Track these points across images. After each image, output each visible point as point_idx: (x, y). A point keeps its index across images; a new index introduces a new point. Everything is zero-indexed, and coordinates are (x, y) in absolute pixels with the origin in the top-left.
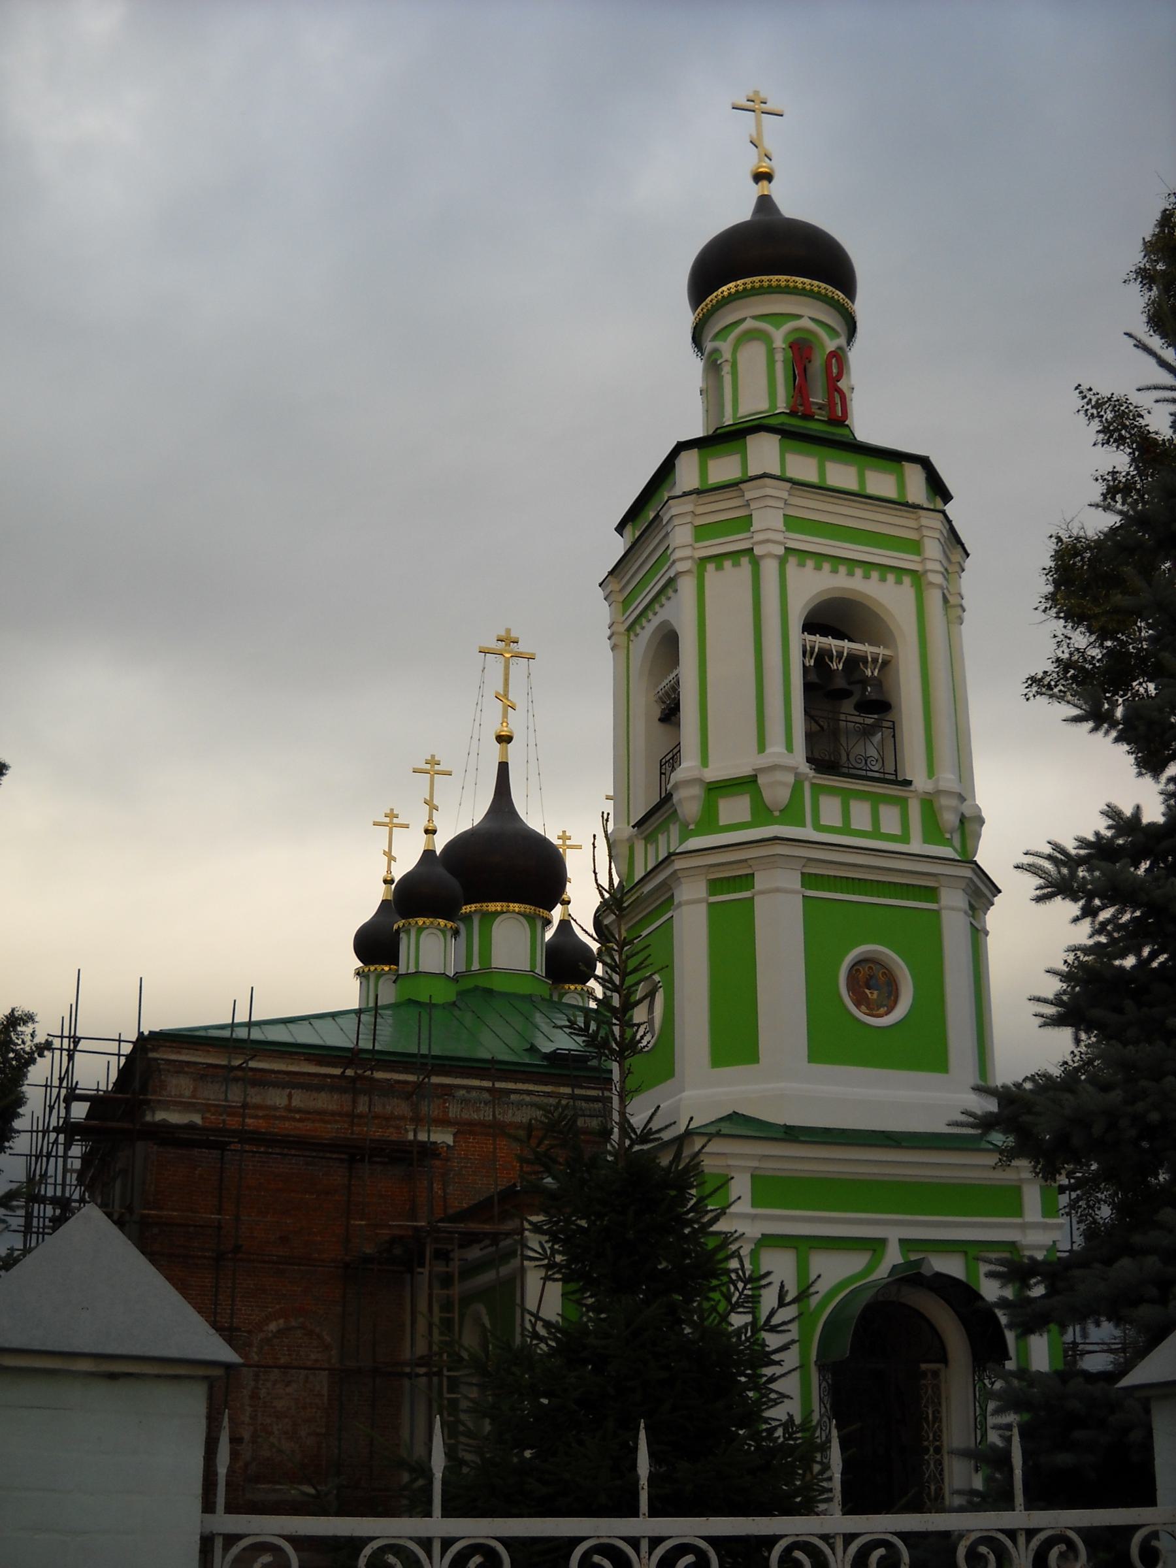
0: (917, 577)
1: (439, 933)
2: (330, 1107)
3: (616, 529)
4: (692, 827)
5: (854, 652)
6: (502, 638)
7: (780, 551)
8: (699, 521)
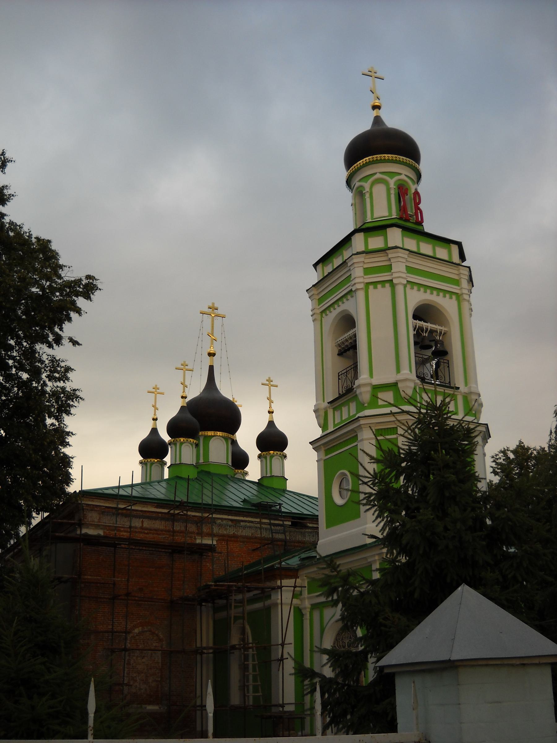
0: (458, 296)
1: (190, 445)
2: (161, 527)
3: (313, 265)
4: (366, 405)
5: (432, 328)
6: (210, 307)
8: (366, 266)
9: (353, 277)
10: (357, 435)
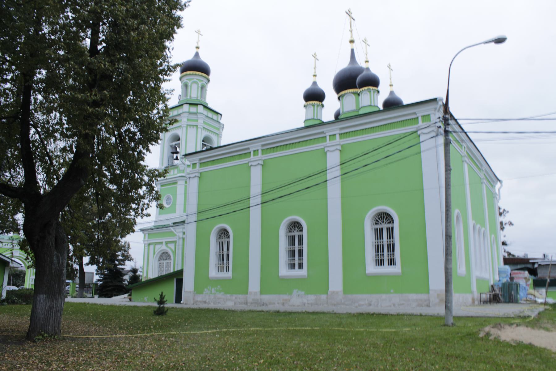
7: (186, 125)
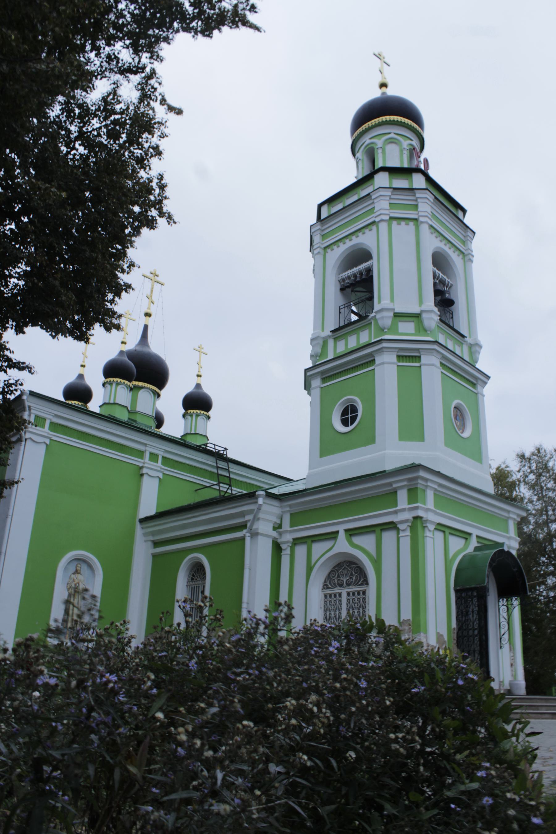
9: (376, 209)
10: (375, 360)
